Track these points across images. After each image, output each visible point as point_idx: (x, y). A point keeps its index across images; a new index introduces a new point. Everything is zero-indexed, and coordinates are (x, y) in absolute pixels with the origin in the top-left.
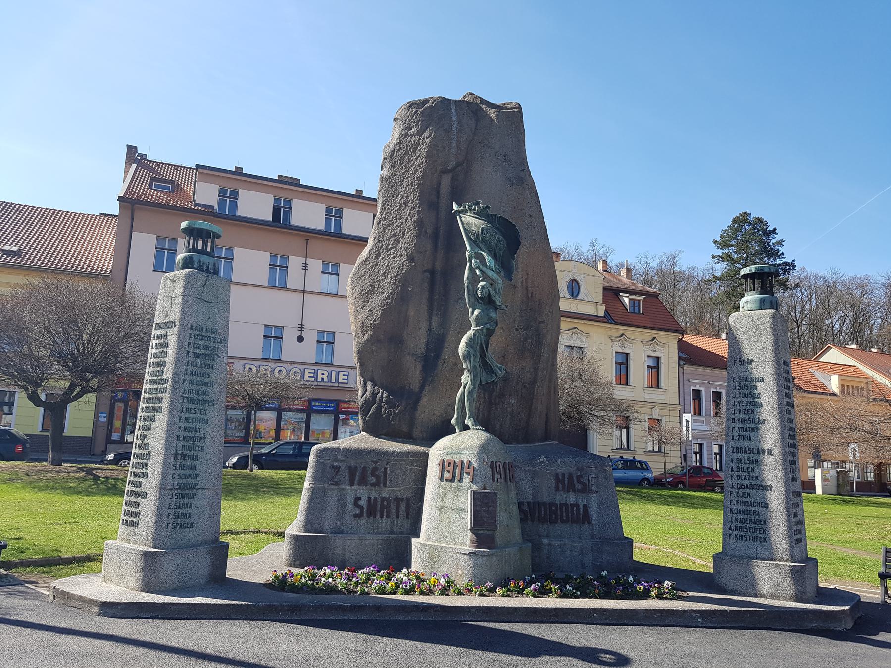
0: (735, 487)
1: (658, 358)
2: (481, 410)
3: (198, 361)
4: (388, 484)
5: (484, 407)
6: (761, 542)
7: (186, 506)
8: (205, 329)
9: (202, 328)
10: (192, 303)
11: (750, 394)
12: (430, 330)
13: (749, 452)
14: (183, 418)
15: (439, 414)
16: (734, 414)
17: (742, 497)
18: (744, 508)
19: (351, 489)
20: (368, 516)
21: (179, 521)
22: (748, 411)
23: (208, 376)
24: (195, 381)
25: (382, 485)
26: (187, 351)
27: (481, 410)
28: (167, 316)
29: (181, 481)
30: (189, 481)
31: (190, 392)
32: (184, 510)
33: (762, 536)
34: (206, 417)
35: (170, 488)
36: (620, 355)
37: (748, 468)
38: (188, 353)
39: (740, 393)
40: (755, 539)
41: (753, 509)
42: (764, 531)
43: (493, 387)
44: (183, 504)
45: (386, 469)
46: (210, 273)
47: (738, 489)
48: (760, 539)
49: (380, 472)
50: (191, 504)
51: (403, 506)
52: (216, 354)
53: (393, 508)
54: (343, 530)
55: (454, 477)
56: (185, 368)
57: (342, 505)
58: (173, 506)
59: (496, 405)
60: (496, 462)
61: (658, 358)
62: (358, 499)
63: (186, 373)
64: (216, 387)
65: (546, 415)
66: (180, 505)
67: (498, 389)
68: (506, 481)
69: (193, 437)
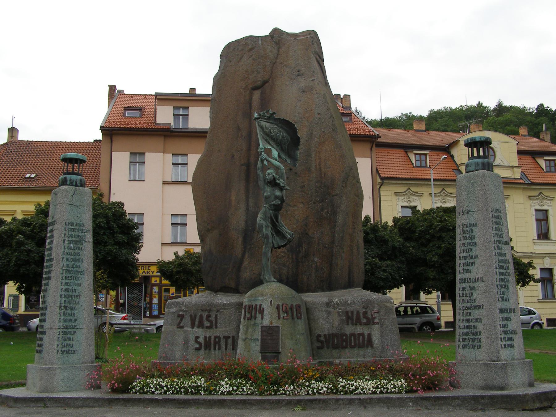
0: (462, 309)
2: (290, 268)
3: (72, 245)
5: (292, 265)
6: (478, 348)
7: (69, 339)
8: (75, 224)
9: (73, 224)
10: (66, 208)
11: (469, 237)
12: (248, 209)
13: (469, 281)
14: (64, 283)
16: (460, 253)
17: (466, 316)
18: (467, 324)
19: (192, 331)
20: (205, 349)
21: (65, 349)
22: (469, 250)
23: (79, 255)
25: (214, 327)
26: (64, 239)
27: (290, 268)
28: (53, 217)
29: (65, 324)
30: (71, 323)
31: (67, 265)
32: (69, 342)
33: (479, 344)
34: (79, 282)
36: (541, 213)
37: (469, 293)
38: (64, 241)
39: (463, 237)
40: (474, 347)
41: (473, 324)
42: (480, 340)
44: (68, 338)
45: (216, 316)
46: (78, 186)
47: (464, 310)
48: (477, 346)
49: (213, 318)
50: (73, 338)
51: (230, 341)
52: (84, 240)
53: (223, 343)
54: (188, 359)
55: (251, 316)
56: (63, 250)
57: (186, 342)
58: (60, 339)
61: (547, 211)
62: (197, 337)
65: (349, 268)
66: (65, 339)
67: (303, 250)
68: (293, 319)
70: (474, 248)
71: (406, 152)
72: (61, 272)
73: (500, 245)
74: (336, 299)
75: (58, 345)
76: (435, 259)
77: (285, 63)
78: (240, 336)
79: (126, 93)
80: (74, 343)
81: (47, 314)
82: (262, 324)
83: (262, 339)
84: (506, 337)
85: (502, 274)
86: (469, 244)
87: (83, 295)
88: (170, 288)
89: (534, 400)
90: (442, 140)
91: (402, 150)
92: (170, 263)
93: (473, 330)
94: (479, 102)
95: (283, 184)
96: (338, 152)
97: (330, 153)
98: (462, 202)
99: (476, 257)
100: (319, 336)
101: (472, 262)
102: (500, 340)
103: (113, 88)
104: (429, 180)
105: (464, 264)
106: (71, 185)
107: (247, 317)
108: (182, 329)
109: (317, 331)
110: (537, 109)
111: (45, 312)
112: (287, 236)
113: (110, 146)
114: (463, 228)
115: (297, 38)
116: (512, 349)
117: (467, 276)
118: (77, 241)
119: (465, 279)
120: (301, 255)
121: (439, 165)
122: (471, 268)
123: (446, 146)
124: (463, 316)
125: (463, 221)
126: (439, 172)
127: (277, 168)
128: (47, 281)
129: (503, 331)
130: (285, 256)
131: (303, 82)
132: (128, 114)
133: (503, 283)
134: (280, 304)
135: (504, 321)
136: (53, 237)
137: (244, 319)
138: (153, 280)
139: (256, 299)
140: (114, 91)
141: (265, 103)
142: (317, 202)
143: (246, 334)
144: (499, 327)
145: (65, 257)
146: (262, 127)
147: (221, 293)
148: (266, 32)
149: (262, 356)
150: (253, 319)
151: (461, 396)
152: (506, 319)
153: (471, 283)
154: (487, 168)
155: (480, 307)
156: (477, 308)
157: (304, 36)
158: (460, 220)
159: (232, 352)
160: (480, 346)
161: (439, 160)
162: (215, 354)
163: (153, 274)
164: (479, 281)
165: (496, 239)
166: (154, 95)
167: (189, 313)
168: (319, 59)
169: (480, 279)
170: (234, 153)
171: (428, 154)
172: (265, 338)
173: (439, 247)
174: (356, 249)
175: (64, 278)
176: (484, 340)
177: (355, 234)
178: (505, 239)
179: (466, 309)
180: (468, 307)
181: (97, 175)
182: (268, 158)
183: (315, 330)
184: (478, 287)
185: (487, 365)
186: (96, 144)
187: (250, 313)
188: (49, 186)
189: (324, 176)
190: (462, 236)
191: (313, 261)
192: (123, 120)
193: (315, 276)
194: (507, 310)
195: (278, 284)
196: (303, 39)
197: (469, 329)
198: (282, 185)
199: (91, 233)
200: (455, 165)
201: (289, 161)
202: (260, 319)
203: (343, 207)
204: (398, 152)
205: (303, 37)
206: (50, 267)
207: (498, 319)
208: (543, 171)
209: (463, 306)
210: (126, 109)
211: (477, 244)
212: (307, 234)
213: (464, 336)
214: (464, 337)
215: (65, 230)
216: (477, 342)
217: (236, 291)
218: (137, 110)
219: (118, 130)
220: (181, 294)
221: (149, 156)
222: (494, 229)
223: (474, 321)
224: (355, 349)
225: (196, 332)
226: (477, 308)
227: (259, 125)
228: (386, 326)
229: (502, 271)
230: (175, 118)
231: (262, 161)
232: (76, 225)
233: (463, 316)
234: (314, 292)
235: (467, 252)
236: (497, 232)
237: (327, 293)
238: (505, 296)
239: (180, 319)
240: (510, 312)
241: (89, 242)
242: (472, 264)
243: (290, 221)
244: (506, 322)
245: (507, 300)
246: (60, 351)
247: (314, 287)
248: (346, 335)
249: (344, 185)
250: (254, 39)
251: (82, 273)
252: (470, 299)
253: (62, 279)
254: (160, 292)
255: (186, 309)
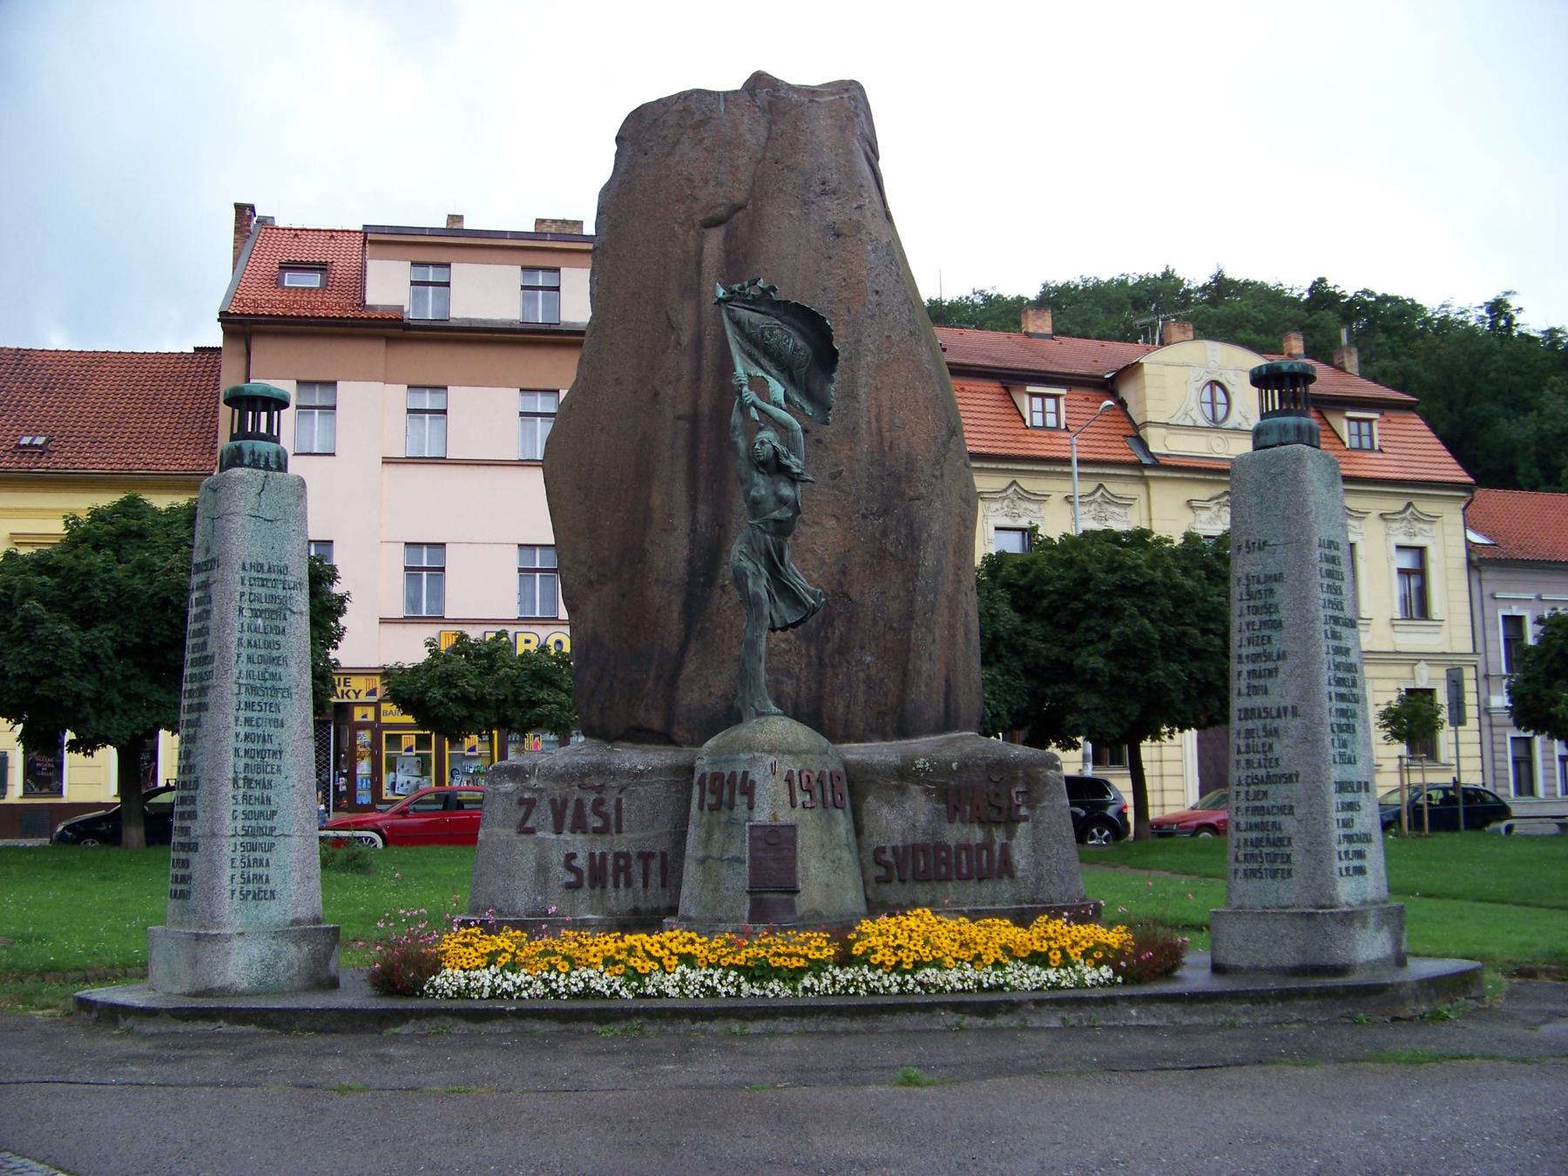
0: (1243, 782)
1: (1420, 551)
2: (804, 679)
3: (260, 621)
4: (624, 828)
5: (809, 673)
8: (266, 568)
9: (262, 566)
11: (1264, 606)
12: (693, 531)
13: (1264, 715)
14: (242, 719)
15: (720, 693)
16: (1240, 646)
18: (1257, 819)
20: (592, 887)
21: (251, 887)
24: (256, 656)
25: (614, 830)
28: (208, 550)
29: (248, 823)
30: (262, 822)
31: (249, 674)
32: (259, 871)
33: (1285, 867)
34: (280, 717)
35: (231, 833)
37: (1264, 745)
38: (241, 610)
41: (1271, 819)
42: (1289, 856)
43: (826, 633)
44: (255, 860)
45: (619, 801)
46: (271, 469)
47: (1248, 785)
51: (655, 865)
53: (637, 870)
55: (720, 802)
56: (238, 635)
57: (542, 869)
58: (238, 863)
59: (833, 666)
60: (800, 773)
61: (1420, 551)
63: (240, 644)
64: (293, 663)
69: (262, 750)
70: (1275, 635)
71: (1007, 390)
72: (236, 691)
73: (1338, 629)
74: (922, 760)
75: (233, 877)
76: (1097, 662)
77: (788, 162)
78: (689, 849)
79: (280, 226)
80: (270, 871)
81: (198, 799)
82: (750, 820)
83: (753, 858)
84: (1351, 849)
85: (1341, 697)
86: (1264, 624)
87: (289, 750)
88: (401, 735)
89: (1417, 996)
90: (1096, 361)
91: (997, 384)
92: (416, 669)
93: (1271, 833)
94: (1167, 266)
95: (798, 467)
96: (924, 388)
97: (903, 391)
98: (1246, 522)
99: (1282, 656)
100: (881, 850)
101: (1270, 667)
102: (1337, 856)
103: (248, 212)
104: (1066, 462)
105: (1252, 673)
106: (254, 467)
107: (709, 805)
108: (532, 837)
109: (875, 839)
110: (1310, 290)
111: (192, 793)
112: (806, 599)
113: (243, 362)
114: (1248, 585)
115: (817, 99)
116: (1361, 878)
117: (1257, 701)
118: (272, 611)
119: (1253, 709)
120: (830, 647)
121: (1094, 423)
122: (1268, 682)
123: (1107, 376)
124: (1248, 800)
125: (1248, 569)
126: (1091, 443)
127: (781, 427)
128: (194, 715)
129: (1344, 836)
130: (790, 650)
131: (835, 211)
132: (291, 280)
133: (1344, 721)
134: (796, 773)
135: (1347, 810)
136: (210, 602)
137: (701, 807)
138: (358, 714)
139: (733, 757)
140: (250, 218)
141: (736, 263)
142: (872, 514)
143: (706, 847)
144: (1336, 826)
145: (244, 652)
146: (738, 324)
147: (624, 744)
148: (731, 80)
149: (752, 901)
150: (724, 808)
151: (1253, 991)
152: (1351, 806)
153: (1268, 721)
154: (1306, 440)
155: (1290, 778)
156: (1283, 780)
157: (832, 94)
158: (1243, 566)
159: (660, 892)
160: (1289, 871)
161: (1094, 411)
162: (617, 898)
163: (357, 697)
164: (1289, 715)
165: (1330, 612)
166: (360, 232)
167: (548, 795)
168: (870, 154)
169: (1290, 709)
170: (658, 388)
171: (1063, 395)
172: (760, 854)
173: (1105, 637)
174: (962, 633)
175: (242, 706)
176: (1300, 858)
177: (960, 596)
178: (1348, 613)
179: (1254, 784)
180: (1260, 777)
181: (209, 441)
182: (759, 402)
183: (871, 835)
184: (1286, 729)
185: (1310, 916)
186: (201, 358)
187: (718, 792)
188: (85, 469)
189: (891, 448)
190: (1245, 604)
191: (860, 662)
192: (277, 296)
193: (866, 702)
194: (1351, 784)
195: (787, 721)
196: (831, 101)
197: (1263, 830)
198: (796, 470)
199: (306, 591)
200: (1128, 426)
201: (809, 410)
202: (745, 807)
203: (936, 528)
204: (986, 389)
205: (832, 98)
206: (202, 679)
207: (1334, 808)
208: (1342, 447)
209: (1248, 777)
210: (289, 266)
211: (1285, 624)
212: (846, 595)
213: (1249, 848)
214: (1249, 850)
215: (243, 584)
216: (1283, 863)
217: (665, 738)
218: (315, 269)
219: (266, 323)
220: (430, 748)
221: (347, 391)
222: (1325, 589)
223: (1275, 810)
224: (971, 883)
225: (567, 842)
226: (1283, 780)
227: (731, 319)
228: (1045, 825)
229: (1343, 690)
230: (415, 294)
231: (744, 409)
232: (269, 570)
233: (1248, 800)
234: (862, 741)
235: (1257, 645)
236: (1332, 597)
237: (894, 742)
238: (1348, 752)
239: (524, 809)
240: (1359, 790)
241: (301, 613)
242: (1271, 673)
243: (803, 561)
244: (1351, 813)
245: (1351, 761)
246: (237, 893)
247: (861, 727)
248: (946, 848)
249: (937, 473)
250: (708, 98)
251: (288, 693)
252: (1265, 759)
253: (237, 710)
254: (375, 745)
255: (541, 786)
